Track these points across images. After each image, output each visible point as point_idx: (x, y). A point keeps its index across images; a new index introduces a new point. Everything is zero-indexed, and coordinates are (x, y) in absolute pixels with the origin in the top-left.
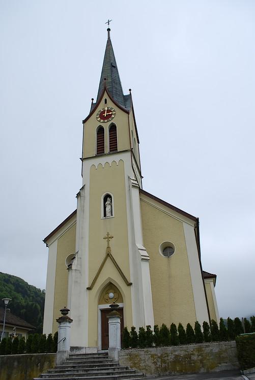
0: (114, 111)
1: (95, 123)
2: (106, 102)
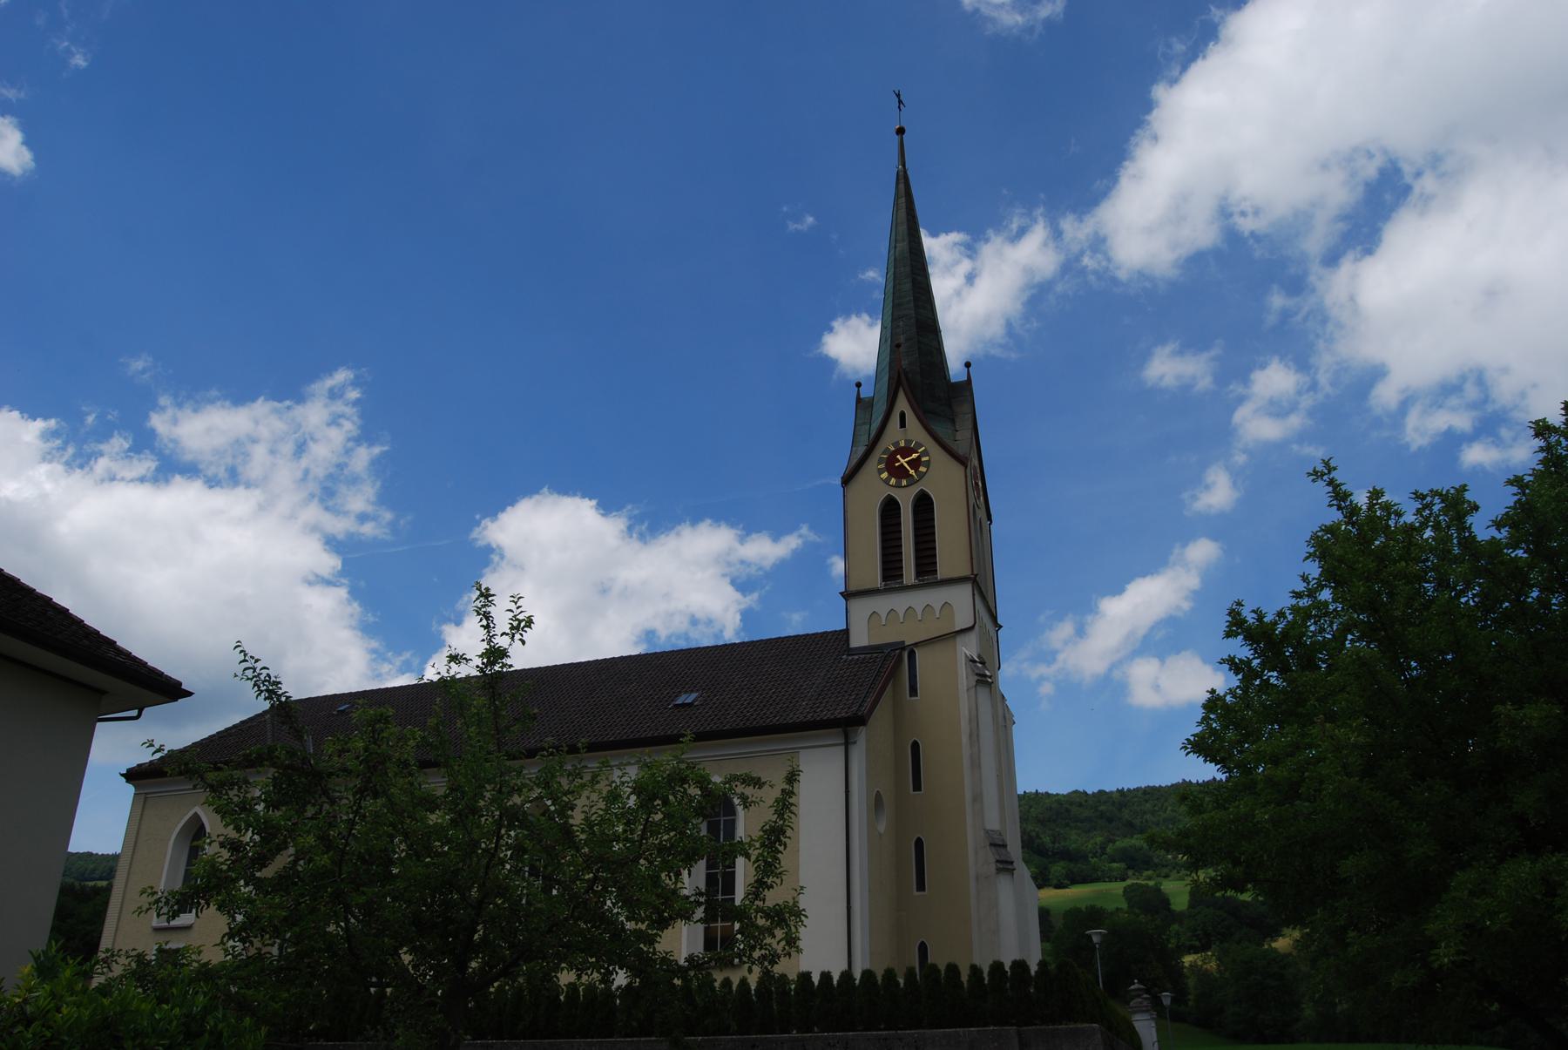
0: (925, 453)
1: (875, 485)
2: (903, 425)
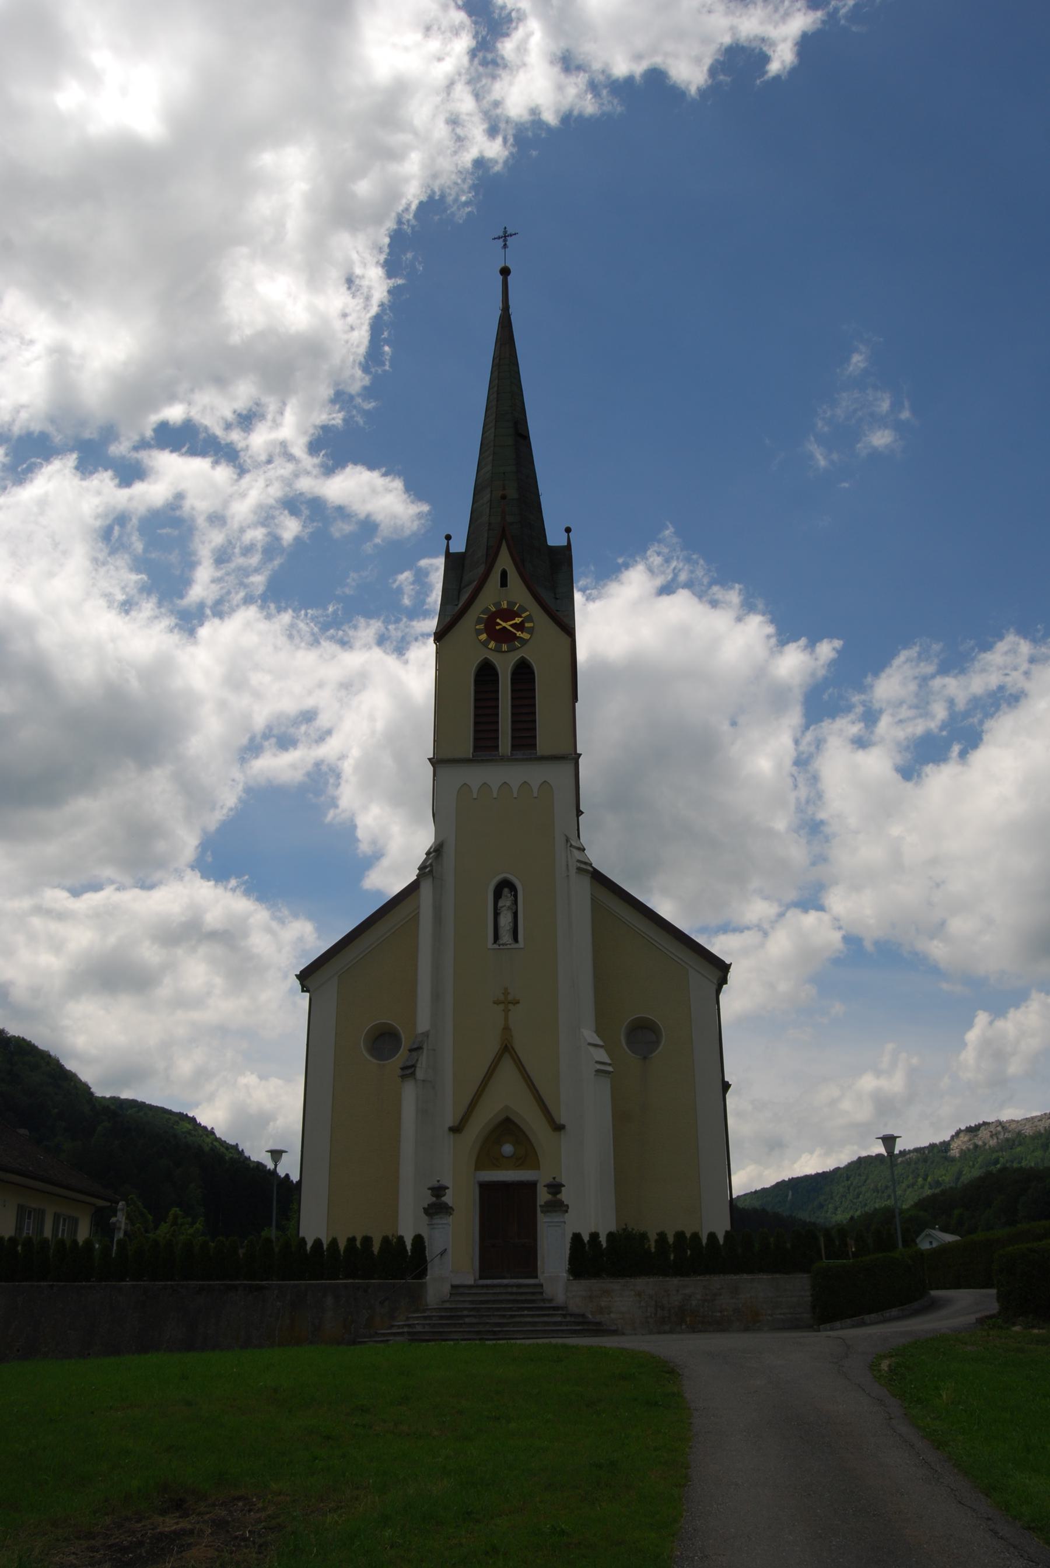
0: (529, 619)
2: (504, 583)
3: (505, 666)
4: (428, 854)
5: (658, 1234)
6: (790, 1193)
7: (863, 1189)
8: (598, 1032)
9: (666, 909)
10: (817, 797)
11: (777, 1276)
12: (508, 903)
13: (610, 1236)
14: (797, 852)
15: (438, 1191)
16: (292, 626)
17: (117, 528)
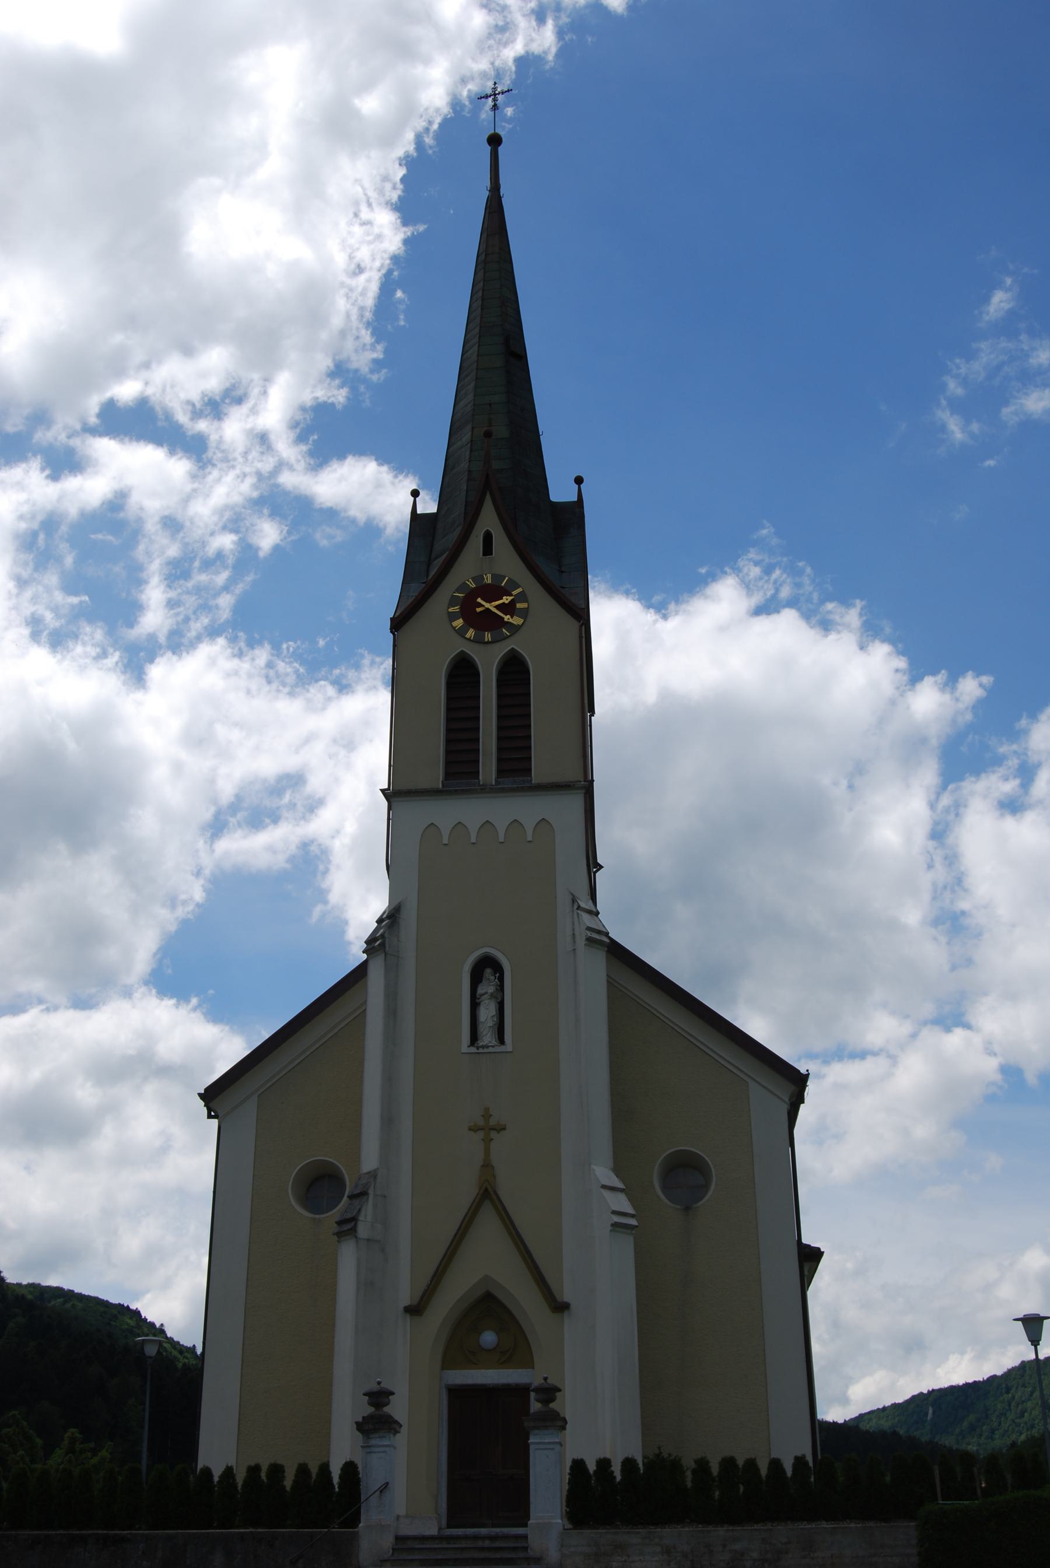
0: (522, 597)
2: (488, 550)
3: (488, 664)
4: (380, 921)
5: (696, 1462)
6: (930, 1411)
7: (1029, 1404)
8: (618, 1170)
9: (757, 1027)
10: (958, 883)
11: (871, 1524)
12: (491, 989)
13: (629, 1464)
14: (933, 953)
15: (379, 1397)
16: (270, 665)
17: (42, 537)
